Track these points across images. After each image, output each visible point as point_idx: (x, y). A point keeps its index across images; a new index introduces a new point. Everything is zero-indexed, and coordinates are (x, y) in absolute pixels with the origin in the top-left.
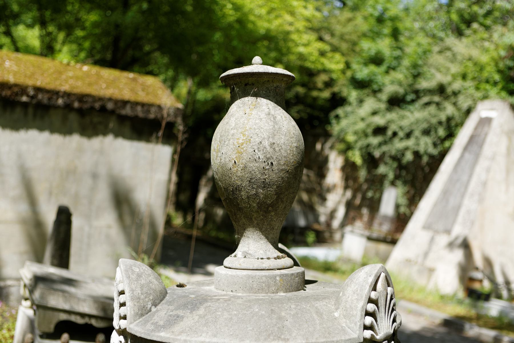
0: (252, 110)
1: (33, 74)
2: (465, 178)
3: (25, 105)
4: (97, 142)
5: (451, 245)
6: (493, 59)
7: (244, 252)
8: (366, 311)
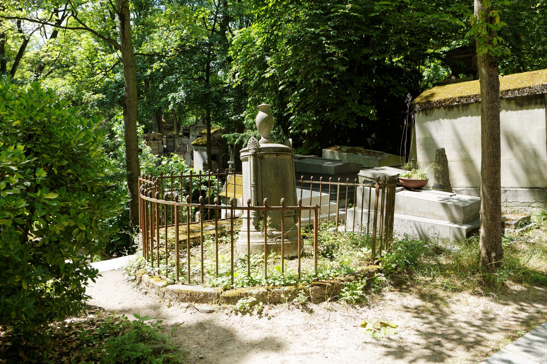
3: (457, 106)
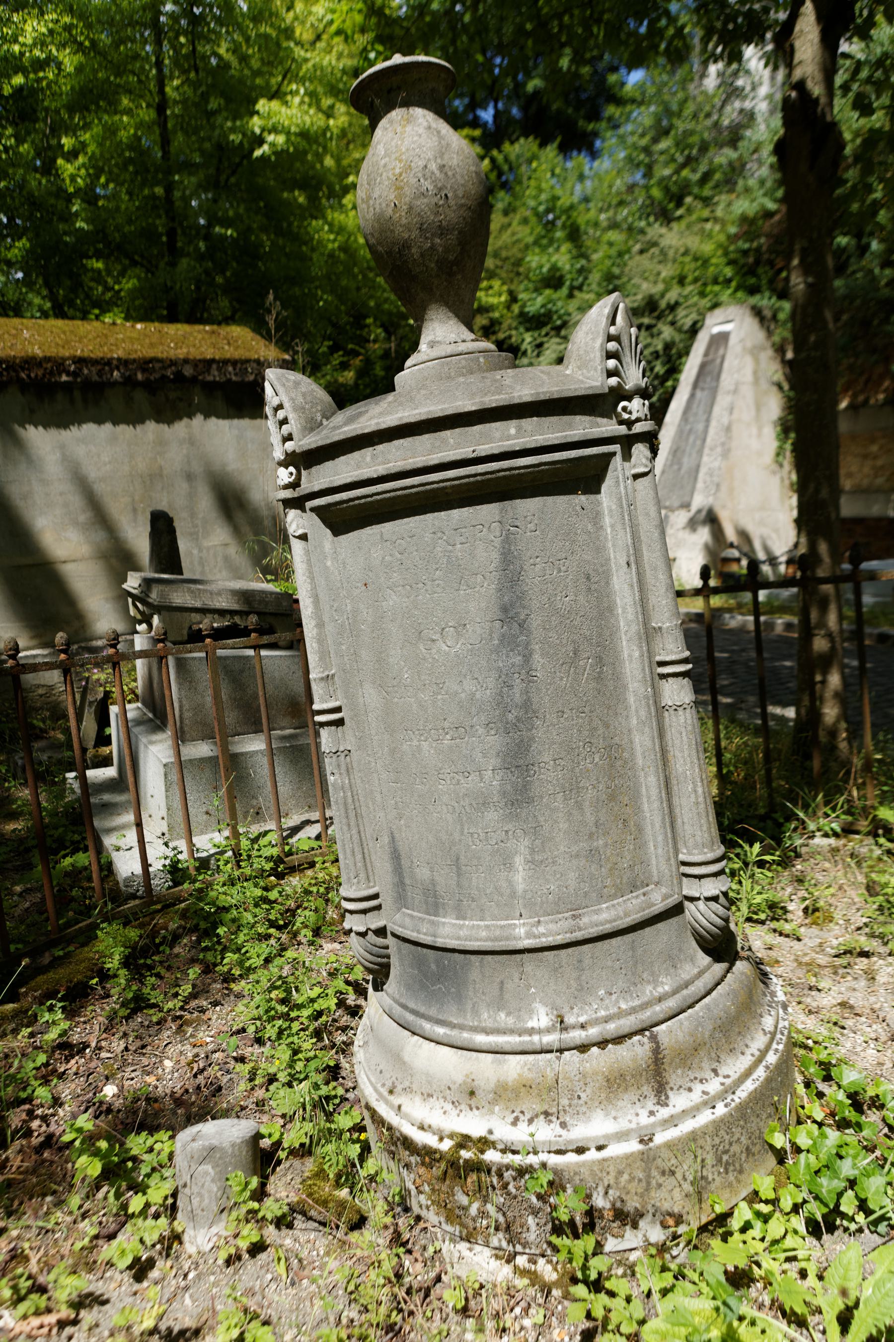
0: (404, 126)
1: (67, 342)
2: (700, 427)
4: (181, 428)
5: (692, 525)
6: (720, 246)
7: (429, 343)
8: (607, 352)
